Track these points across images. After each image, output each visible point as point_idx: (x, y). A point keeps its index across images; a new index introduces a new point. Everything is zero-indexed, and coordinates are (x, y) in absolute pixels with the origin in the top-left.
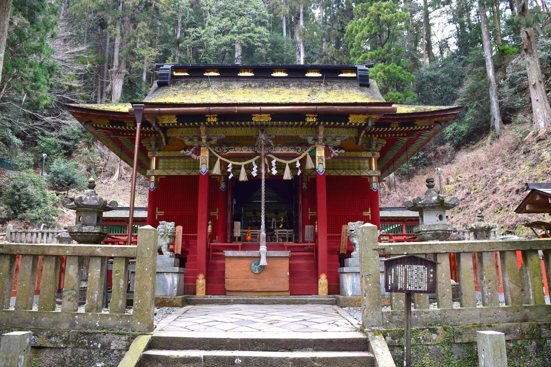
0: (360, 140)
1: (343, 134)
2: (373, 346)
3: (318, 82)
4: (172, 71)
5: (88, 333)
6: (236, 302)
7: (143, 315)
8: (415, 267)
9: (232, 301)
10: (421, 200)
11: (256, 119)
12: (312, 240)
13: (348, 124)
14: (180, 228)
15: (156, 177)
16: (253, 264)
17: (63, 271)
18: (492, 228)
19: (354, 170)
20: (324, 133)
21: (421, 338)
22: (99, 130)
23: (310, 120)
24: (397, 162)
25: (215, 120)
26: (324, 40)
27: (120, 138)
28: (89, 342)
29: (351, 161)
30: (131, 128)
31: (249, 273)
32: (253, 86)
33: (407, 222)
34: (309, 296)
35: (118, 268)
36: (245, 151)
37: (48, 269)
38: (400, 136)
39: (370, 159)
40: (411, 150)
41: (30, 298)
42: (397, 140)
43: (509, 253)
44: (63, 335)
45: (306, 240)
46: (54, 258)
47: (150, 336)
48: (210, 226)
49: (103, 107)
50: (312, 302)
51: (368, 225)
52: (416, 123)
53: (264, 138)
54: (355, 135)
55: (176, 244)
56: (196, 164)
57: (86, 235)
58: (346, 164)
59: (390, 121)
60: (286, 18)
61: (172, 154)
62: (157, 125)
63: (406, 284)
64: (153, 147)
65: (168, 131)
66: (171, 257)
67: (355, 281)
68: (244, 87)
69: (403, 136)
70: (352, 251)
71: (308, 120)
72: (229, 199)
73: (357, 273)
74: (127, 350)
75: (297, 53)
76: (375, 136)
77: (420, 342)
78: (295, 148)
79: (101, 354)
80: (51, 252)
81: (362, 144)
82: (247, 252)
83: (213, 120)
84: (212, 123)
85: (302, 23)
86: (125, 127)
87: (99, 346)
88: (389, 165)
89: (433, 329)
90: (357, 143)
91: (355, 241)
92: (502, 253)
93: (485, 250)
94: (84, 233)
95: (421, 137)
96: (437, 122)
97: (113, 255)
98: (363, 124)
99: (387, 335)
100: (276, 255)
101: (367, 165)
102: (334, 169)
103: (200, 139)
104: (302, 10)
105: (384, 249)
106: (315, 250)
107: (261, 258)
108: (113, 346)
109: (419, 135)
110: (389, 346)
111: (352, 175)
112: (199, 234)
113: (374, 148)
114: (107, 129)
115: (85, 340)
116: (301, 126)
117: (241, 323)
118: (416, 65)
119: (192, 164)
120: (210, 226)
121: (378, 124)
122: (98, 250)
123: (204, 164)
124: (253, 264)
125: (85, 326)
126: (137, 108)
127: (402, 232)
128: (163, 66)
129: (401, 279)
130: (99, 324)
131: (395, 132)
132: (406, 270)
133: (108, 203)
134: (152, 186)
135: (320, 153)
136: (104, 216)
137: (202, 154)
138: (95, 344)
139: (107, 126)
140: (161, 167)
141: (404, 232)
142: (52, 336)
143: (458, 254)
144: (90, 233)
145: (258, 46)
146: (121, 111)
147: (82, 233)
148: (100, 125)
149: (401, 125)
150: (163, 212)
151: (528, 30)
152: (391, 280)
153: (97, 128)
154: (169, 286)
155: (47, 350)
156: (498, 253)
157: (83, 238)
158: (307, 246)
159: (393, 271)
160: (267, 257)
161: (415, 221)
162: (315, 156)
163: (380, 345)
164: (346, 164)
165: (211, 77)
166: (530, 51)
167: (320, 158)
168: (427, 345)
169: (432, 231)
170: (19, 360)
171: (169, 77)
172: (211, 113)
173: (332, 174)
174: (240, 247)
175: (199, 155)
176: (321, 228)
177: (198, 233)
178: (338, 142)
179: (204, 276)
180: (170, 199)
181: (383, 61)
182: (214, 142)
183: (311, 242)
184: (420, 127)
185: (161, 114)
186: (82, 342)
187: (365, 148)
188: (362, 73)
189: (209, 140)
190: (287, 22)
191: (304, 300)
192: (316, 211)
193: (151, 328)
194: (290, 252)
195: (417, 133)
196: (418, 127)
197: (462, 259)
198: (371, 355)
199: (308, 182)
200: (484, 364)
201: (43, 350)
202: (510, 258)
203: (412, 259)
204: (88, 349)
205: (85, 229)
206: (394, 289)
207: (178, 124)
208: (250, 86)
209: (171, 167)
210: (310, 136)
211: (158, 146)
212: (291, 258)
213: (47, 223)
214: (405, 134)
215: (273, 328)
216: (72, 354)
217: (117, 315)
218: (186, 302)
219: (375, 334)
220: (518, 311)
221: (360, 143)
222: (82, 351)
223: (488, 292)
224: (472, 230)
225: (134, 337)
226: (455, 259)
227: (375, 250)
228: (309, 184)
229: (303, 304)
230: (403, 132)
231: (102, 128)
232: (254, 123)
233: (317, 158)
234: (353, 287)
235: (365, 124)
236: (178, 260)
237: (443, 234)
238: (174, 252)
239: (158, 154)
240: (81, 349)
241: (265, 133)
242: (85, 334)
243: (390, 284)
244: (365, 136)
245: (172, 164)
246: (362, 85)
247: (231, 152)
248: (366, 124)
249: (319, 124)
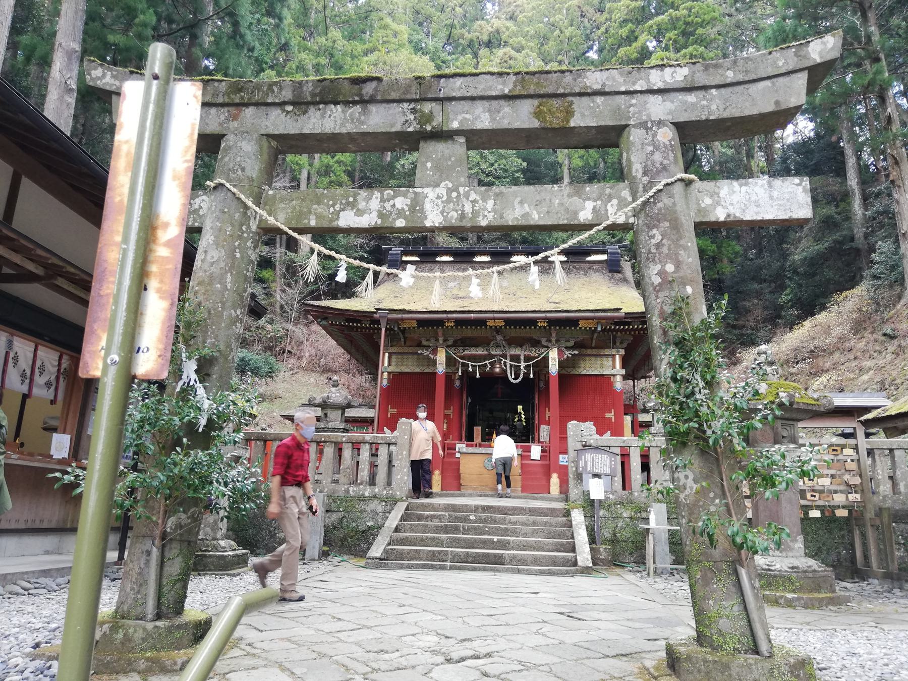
8: (600, 456)
15: (389, 373)
25: (453, 324)
27: (353, 334)
36: (480, 352)
56: (434, 363)
61: (406, 350)
72: (465, 398)
103: (437, 340)
129: (589, 464)
136: (640, 419)
140: (393, 364)
167: (554, 359)
172: (448, 319)
182: (450, 343)
185: (403, 320)
189: (445, 341)
239: (392, 350)
247: (467, 352)
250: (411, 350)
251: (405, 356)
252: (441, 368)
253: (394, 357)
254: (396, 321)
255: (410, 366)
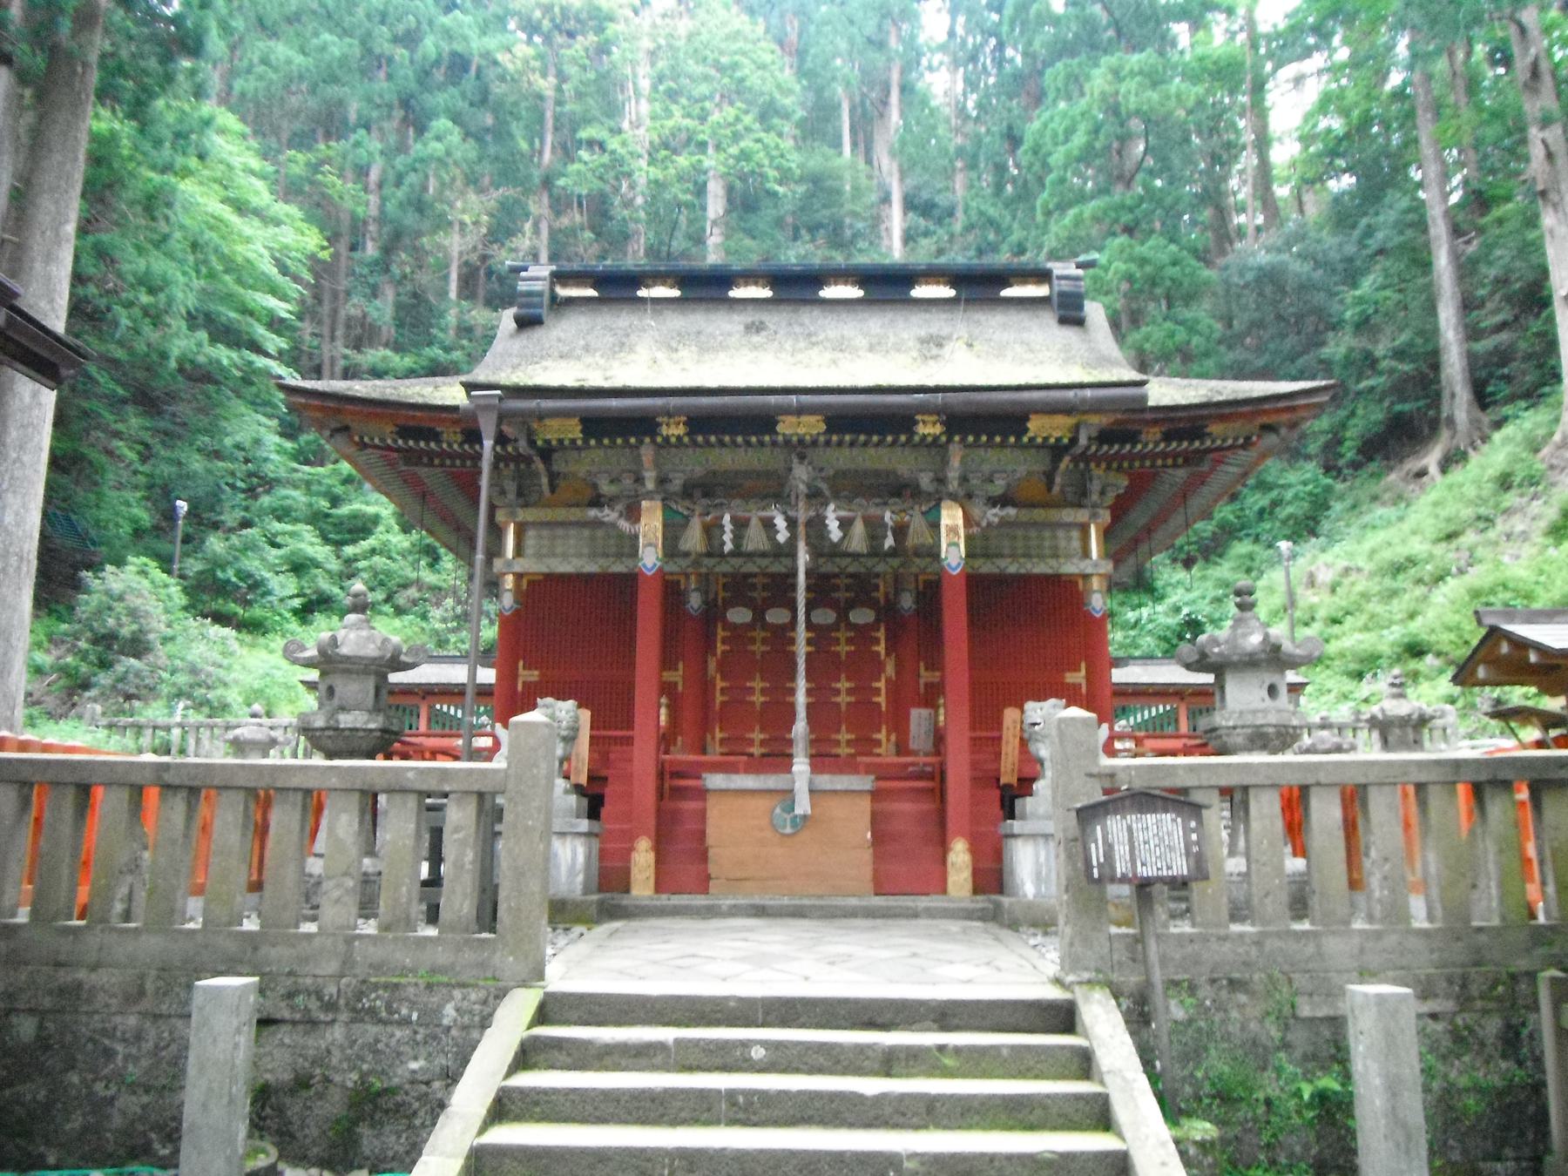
0: (1058, 480)
1: (1009, 465)
4: (552, 284)
6: (734, 912)
8: (1151, 818)
9: (724, 908)
13: (1025, 439)
14: (585, 715)
16: (778, 810)
17: (262, 831)
18: (1433, 718)
19: (1041, 557)
20: (962, 462)
23: (926, 431)
25: (680, 430)
29: (1033, 533)
30: (456, 446)
31: (769, 834)
33: (1194, 700)
35: (459, 818)
37: (227, 820)
38: (1165, 466)
39: (1084, 529)
40: (1196, 503)
42: (1156, 474)
43: (1438, 788)
45: (913, 745)
46: (299, 796)
48: (663, 711)
50: (931, 914)
51: (1076, 712)
52: (1208, 430)
54: (1043, 468)
56: (630, 546)
58: (1020, 544)
60: (851, 100)
61: (561, 514)
62: (532, 443)
64: (511, 496)
65: (555, 456)
67: (1042, 859)
69: (1175, 466)
70: (1034, 780)
71: (922, 430)
73: (1047, 837)
76: (1098, 466)
79: (419, 1037)
81: (1063, 486)
82: (762, 777)
83: (675, 430)
84: (673, 440)
85: (895, 117)
86: (439, 442)
91: (1043, 751)
92: (1420, 787)
93: (1372, 779)
96: (1268, 428)
97: (447, 788)
98: (1066, 441)
100: (839, 787)
103: (639, 480)
104: (895, 77)
105: (1112, 776)
106: (937, 778)
107: (799, 799)
112: (636, 733)
113: (1095, 497)
114: (389, 448)
116: (903, 445)
117: (761, 961)
118: (1224, 235)
121: (1105, 437)
123: (650, 545)
124: (778, 810)
126: (482, 402)
127: (1177, 729)
128: (526, 269)
131: (1154, 456)
134: (508, 600)
135: (951, 516)
137: (643, 521)
140: (529, 551)
141: (1184, 727)
143: (1304, 790)
144: (357, 730)
147: (336, 729)
149: (1167, 437)
150: (536, 673)
151: (1546, 134)
153: (363, 446)
154: (564, 869)
156: (1411, 790)
161: (1202, 699)
166: (1553, 196)
167: (953, 530)
171: (546, 299)
174: (741, 766)
175: (638, 520)
176: (953, 715)
177: (636, 726)
179: (653, 845)
180: (562, 635)
181: (1129, 230)
182: (676, 484)
184: (1219, 442)
185: (541, 416)
187: (1070, 497)
188: (1065, 286)
189: (662, 481)
190: (852, 110)
192: (942, 669)
194: (872, 777)
195: (1211, 456)
197: (1315, 803)
199: (918, 593)
201: (274, 1028)
202: (1436, 798)
205: (346, 720)
207: (586, 441)
211: (525, 497)
212: (876, 795)
216: (348, 1036)
217: (458, 937)
220: (1458, 939)
221: (1056, 489)
223: (1382, 888)
224: (1373, 722)
225: (501, 994)
228: (920, 597)
231: (376, 447)
233: (943, 530)
234: (1038, 875)
236: (585, 802)
237: (1279, 734)
239: (524, 515)
246: (1063, 321)
248: (1074, 441)
249: (950, 440)
250: (575, 514)
251: (560, 532)
252: (650, 558)
253: (531, 533)
254: (524, 418)
255: (571, 559)
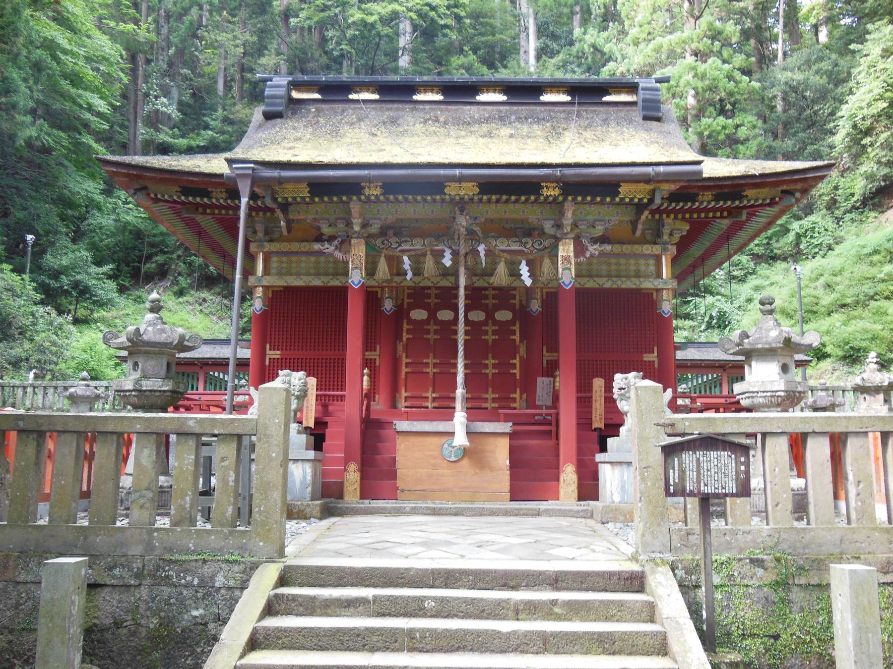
0: (640, 227)
2: (653, 584)
3: (564, 111)
4: (289, 91)
5: (176, 561)
7: (269, 530)
8: (713, 454)
10: (748, 337)
11: (452, 190)
12: (550, 403)
13: (617, 199)
14: (312, 381)
19: (628, 277)
20: (573, 213)
21: (736, 574)
22: (160, 204)
23: (549, 194)
24: (710, 263)
25: (378, 192)
26: (578, 9)
27: (199, 218)
28: (178, 576)
29: (623, 261)
30: (221, 201)
32: (442, 119)
34: (544, 503)
38: (714, 217)
39: (658, 259)
41: (74, 505)
44: (134, 565)
47: (281, 565)
48: (365, 378)
49: (168, 163)
50: (548, 513)
52: (745, 194)
53: (464, 224)
54: (629, 218)
55: (305, 410)
57: (147, 396)
58: (613, 267)
59: (695, 191)
61: (295, 246)
62: (275, 200)
63: (699, 482)
64: (261, 235)
65: (291, 208)
66: (299, 432)
67: (625, 478)
68: (425, 121)
69: (722, 217)
74: (243, 589)
75: (523, 36)
76: (668, 216)
77: (734, 581)
78: (521, 242)
80: (110, 428)
83: (374, 192)
84: (373, 198)
87: (196, 582)
88: (694, 267)
89: (758, 560)
90: (634, 232)
94: (145, 391)
95: (754, 219)
97: (216, 432)
98: (645, 200)
99: (677, 568)
100: (487, 430)
101: (652, 268)
102: (590, 276)
103: (349, 224)
105: (673, 425)
108: (219, 581)
109: (751, 215)
110: (680, 586)
111: (623, 286)
113: (666, 237)
114: (175, 202)
115: (171, 573)
119: (331, 265)
120: (365, 378)
121: (673, 197)
122: (191, 423)
123: (356, 268)
125: (170, 550)
129: (691, 476)
130: (194, 546)
131: (707, 210)
132: (698, 460)
133: (187, 338)
137: (353, 251)
138: (189, 578)
139: (175, 198)
140: (273, 271)
142: (115, 566)
143: (804, 436)
144: (155, 391)
145: (446, 26)
146: (202, 170)
147: (140, 391)
148: (163, 196)
149: (717, 198)
152: (674, 477)
153: (156, 200)
155: (107, 590)
157: (145, 401)
158: (540, 415)
159: (676, 462)
160: (470, 434)
162: (557, 256)
163: (664, 582)
164: (613, 267)
165: (365, 101)
167: (567, 259)
168: (747, 586)
169: (767, 392)
170: (73, 602)
172: (370, 180)
173: (586, 286)
176: (565, 382)
178: (599, 230)
183: (548, 408)
184: (752, 202)
185: (281, 181)
186: (167, 577)
188: (649, 95)
191: (535, 510)
192: (557, 350)
193: (281, 554)
194: (511, 424)
196: (749, 201)
198: (650, 599)
200: (842, 617)
203: (711, 442)
204: (176, 586)
205: (147, 385)
206: (681, 492)
208: (437, 120)
209: (293, 271)
210: (548, 219)
211: (270, 235)
212: (512, 436)
213: (42, 369)
214: (725, 214)
215: (484, 553)
217: (225, 530)
218: (328, 512)
219: (657, 565)
222: (166, 590)
225: (254, 567)
226: (838, 441)
227: (658, 425)
229: (533, 515)
230: (721, 210)
231: (166, 201)
232: (447, 197)
233: (560, 259)
234: (623, 487)
235: (649, 200)
238: (301, 423)
239: (268, 247)
240: (164, 588)
241: (467, 214)
242: (170, 562)
243: (672, 483)
244: (650, 217)
245: (294, 265)
248: (651, 201)
249: (565, 200)
253: (274, 259)
254: (268, 183)
